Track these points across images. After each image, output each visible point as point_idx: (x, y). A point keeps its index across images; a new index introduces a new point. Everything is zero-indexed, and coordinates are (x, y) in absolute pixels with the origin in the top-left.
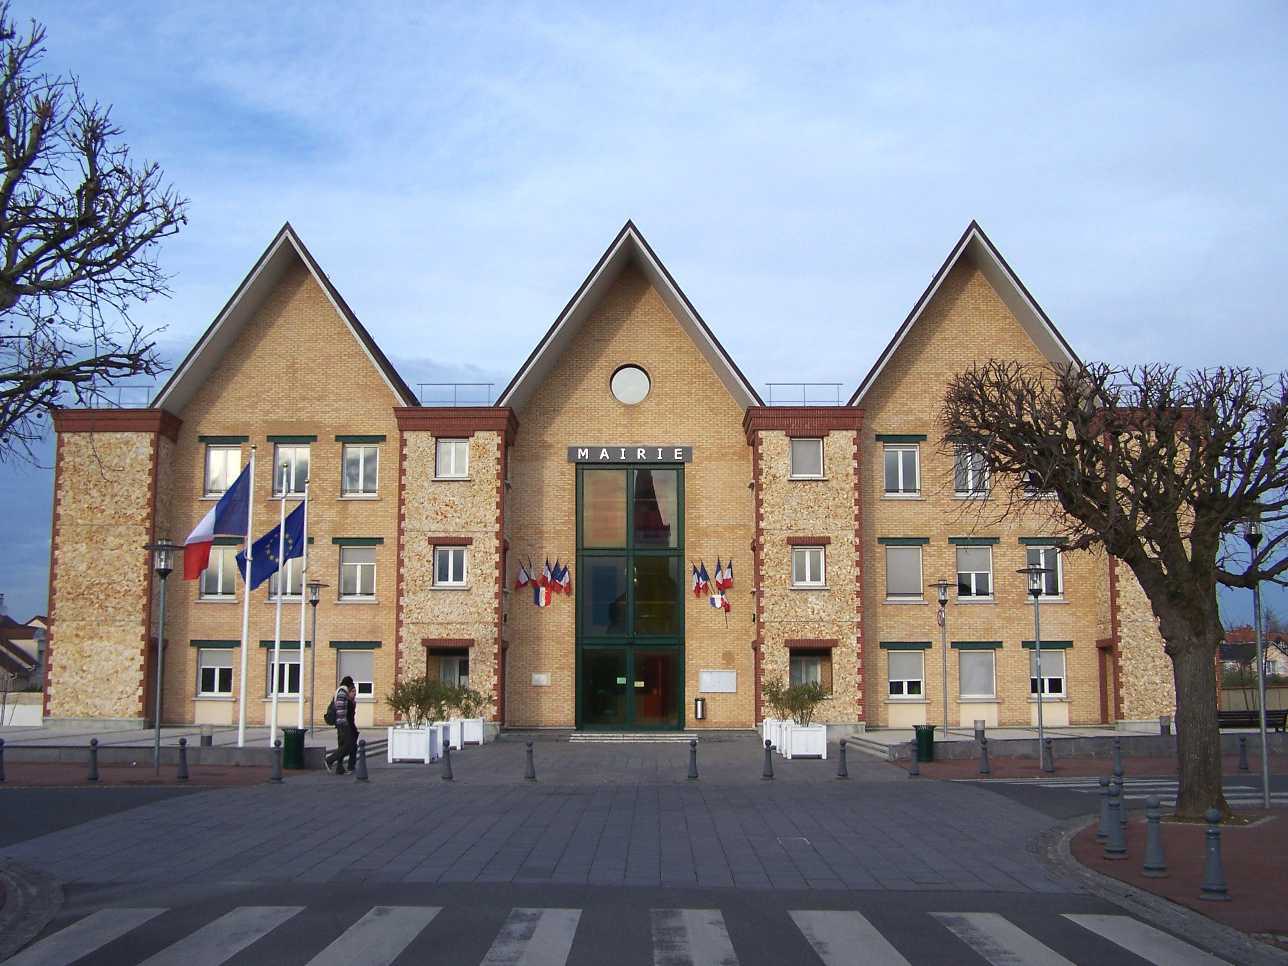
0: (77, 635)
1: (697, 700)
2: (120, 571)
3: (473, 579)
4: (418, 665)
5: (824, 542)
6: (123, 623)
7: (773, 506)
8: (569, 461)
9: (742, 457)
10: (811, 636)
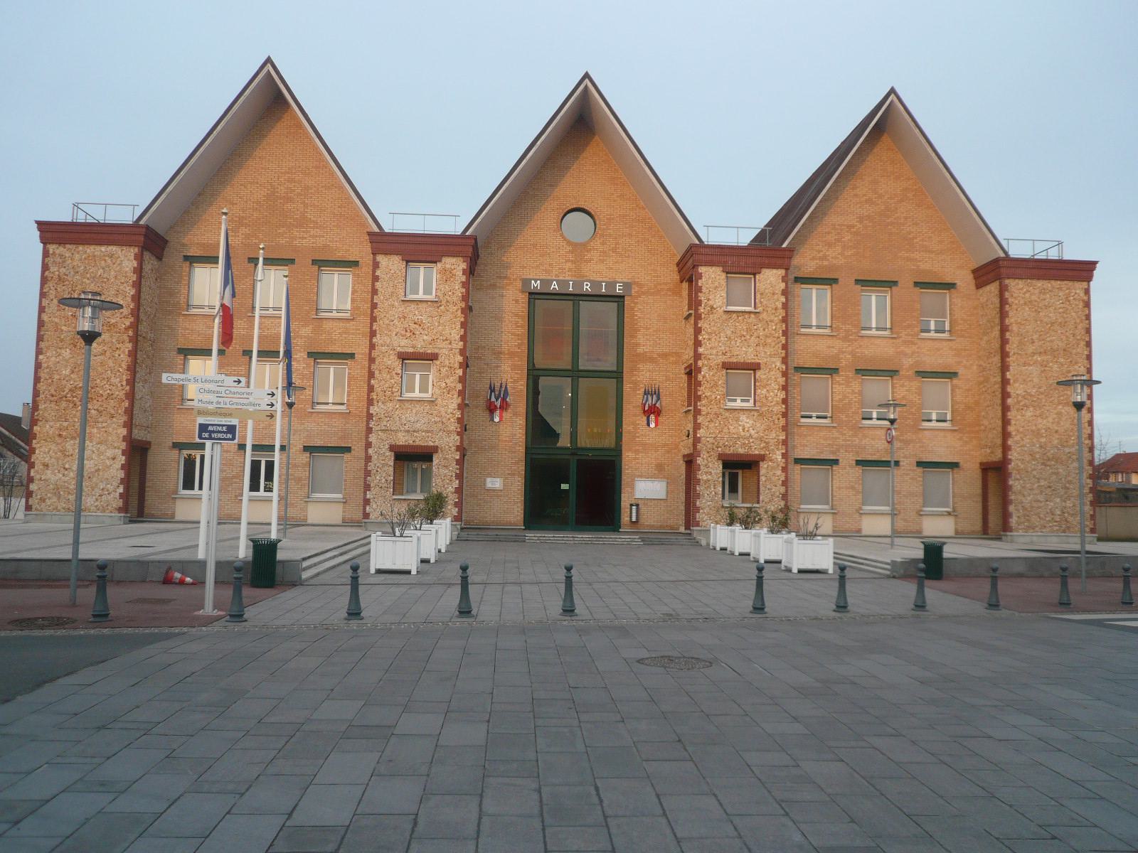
0: (60, 435)
1: (631, 505)
2: (103, 376)
3: (438, 392)
4: (386, 468)
5: (755, 367)
6: (104, 425)
7: (710, 334)
8: (523, 292)
9: (677, 292)
10: (741, 451)
